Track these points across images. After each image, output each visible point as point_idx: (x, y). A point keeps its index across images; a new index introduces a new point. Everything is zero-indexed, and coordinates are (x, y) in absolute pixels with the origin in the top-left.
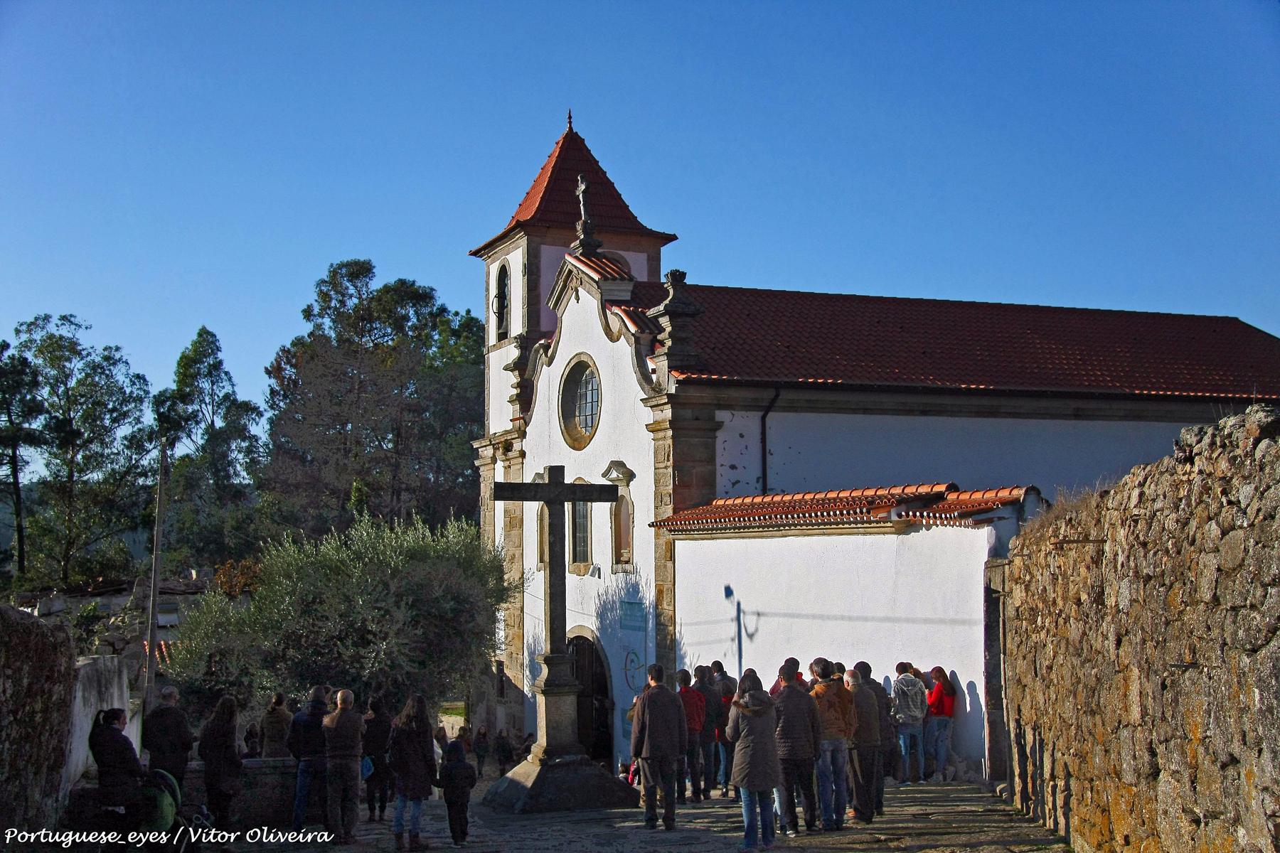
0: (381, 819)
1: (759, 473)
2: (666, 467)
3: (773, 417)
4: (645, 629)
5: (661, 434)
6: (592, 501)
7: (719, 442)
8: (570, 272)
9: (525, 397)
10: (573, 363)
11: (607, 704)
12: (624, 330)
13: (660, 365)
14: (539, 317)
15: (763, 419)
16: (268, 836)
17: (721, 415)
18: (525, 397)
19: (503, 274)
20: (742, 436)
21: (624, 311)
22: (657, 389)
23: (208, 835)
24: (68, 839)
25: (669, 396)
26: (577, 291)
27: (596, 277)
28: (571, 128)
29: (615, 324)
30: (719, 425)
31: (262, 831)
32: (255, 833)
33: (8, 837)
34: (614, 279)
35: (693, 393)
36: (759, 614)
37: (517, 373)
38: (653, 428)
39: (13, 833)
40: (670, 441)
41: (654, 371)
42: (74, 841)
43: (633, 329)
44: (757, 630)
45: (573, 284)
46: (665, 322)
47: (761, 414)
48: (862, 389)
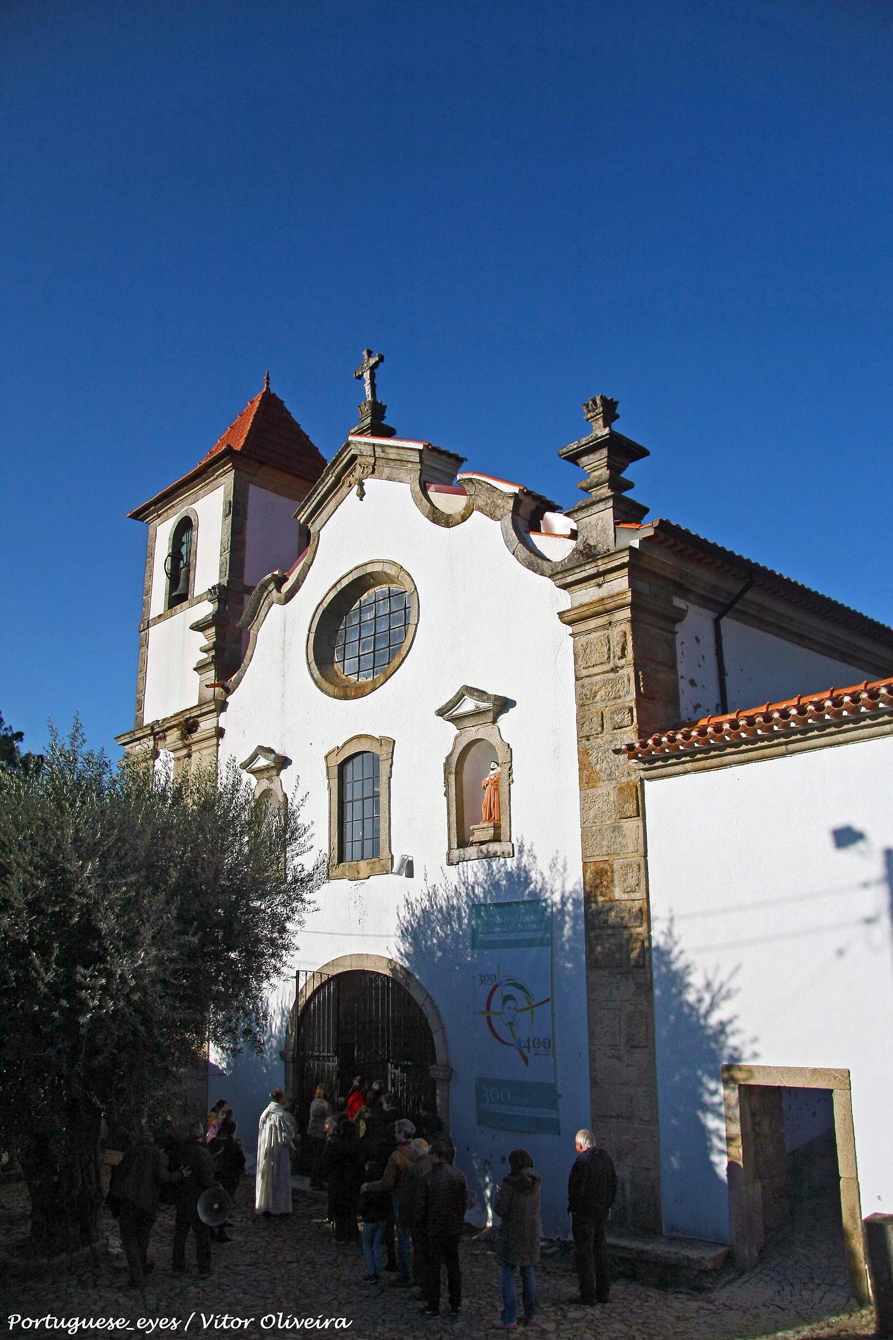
7: (679, 638)
16: (282, 1322)
19: (186, 526)
23: (220, 1321)
24: (74, 1325)
31: (277, 1317)
32: (270, 1319)
33: (12, 1323)
39: (16, 1319)
42: (80, 1327)
45: (358, 473)
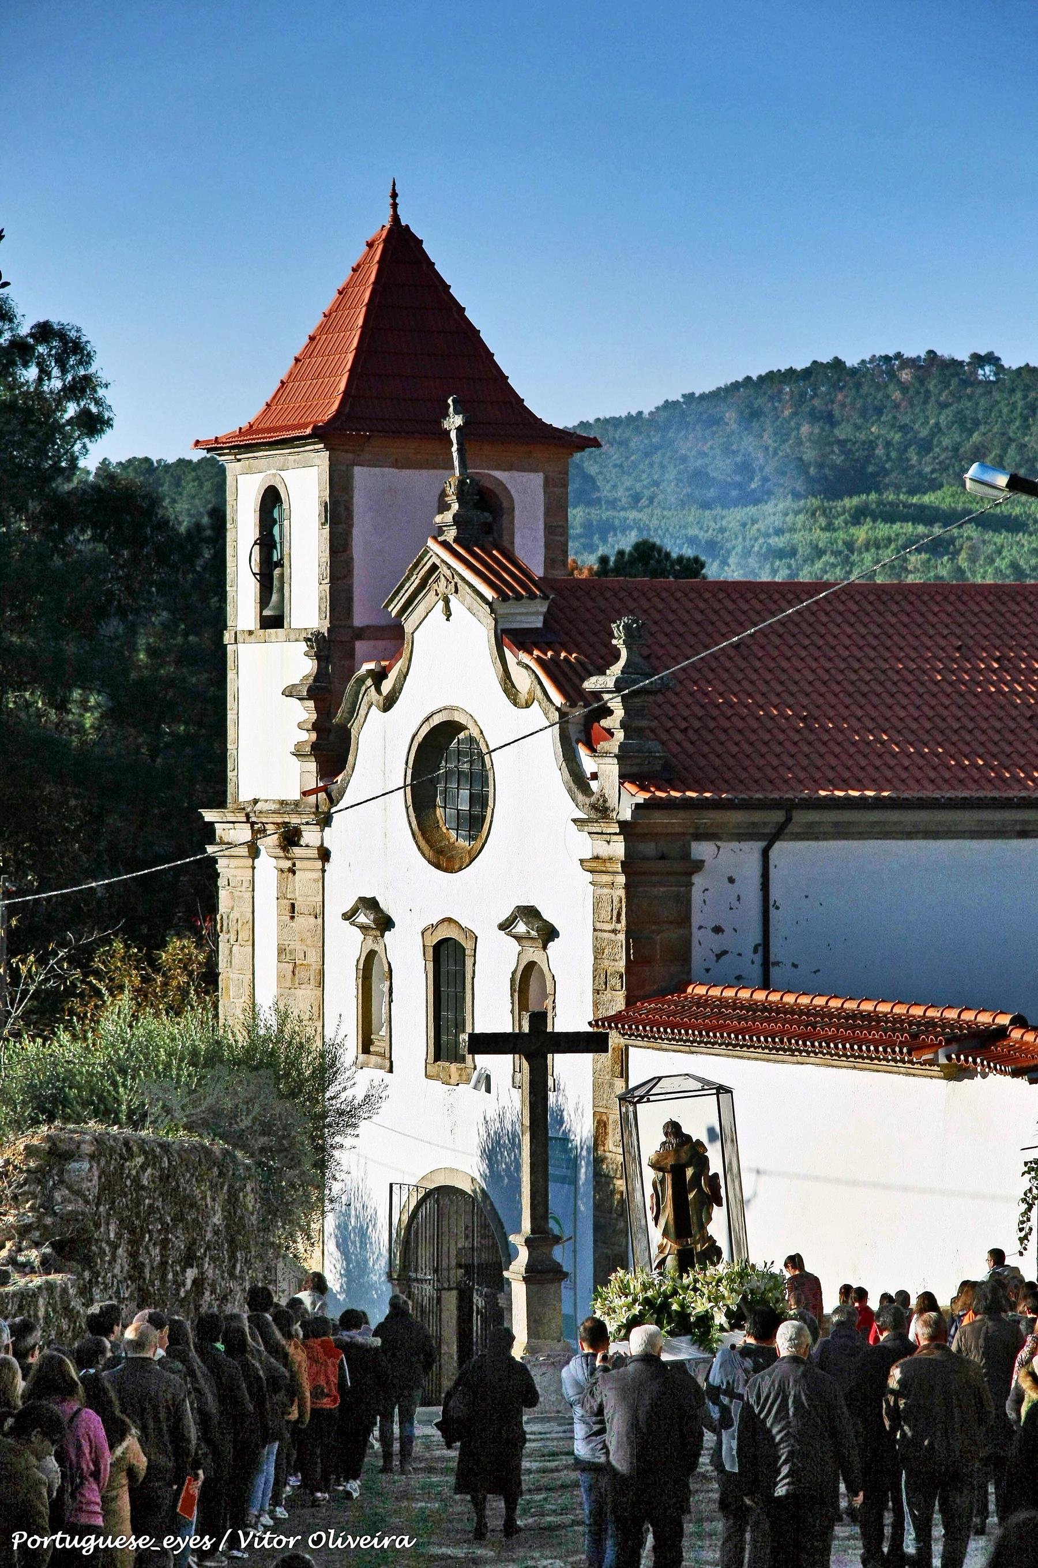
0: (510, 1529)
1: (757, 938)
2: (614, 931)
3: (780, 848)
4: (574, 1181)
5: (606, 878)
6: (553, 1053)
8: (434, 568)
9: (331, 750)
10: (436, 720)
11: (502, 1303)
12: (539, 693)
13: (603, 768)
14: (350, 600)
15: (765, 853)
17: (702, 850)
18: (331, 750)
20: (731, 880)
21: (539, 661)
22: (602, 810)
23: (261, 1539)
25: (622, 824)
26: (447, 601)
27: (489, 594)
28: (396, 218)
29: (523, 681)
30: (698, 866)
32: (320, 1537)
33: (16, 1542)
34: (518, 597)
35: (660, 819)
36: (758, 1172)
37: (311, 704)
38: (594, 865)
39: (21, 1536)
40: (622, 893)
41: (595, 776)
42: (96, 1547)
43: (558, 699)
44: (755, 1195)
46: (616, 705)
47: (762, 844)
48: (922, 804)
